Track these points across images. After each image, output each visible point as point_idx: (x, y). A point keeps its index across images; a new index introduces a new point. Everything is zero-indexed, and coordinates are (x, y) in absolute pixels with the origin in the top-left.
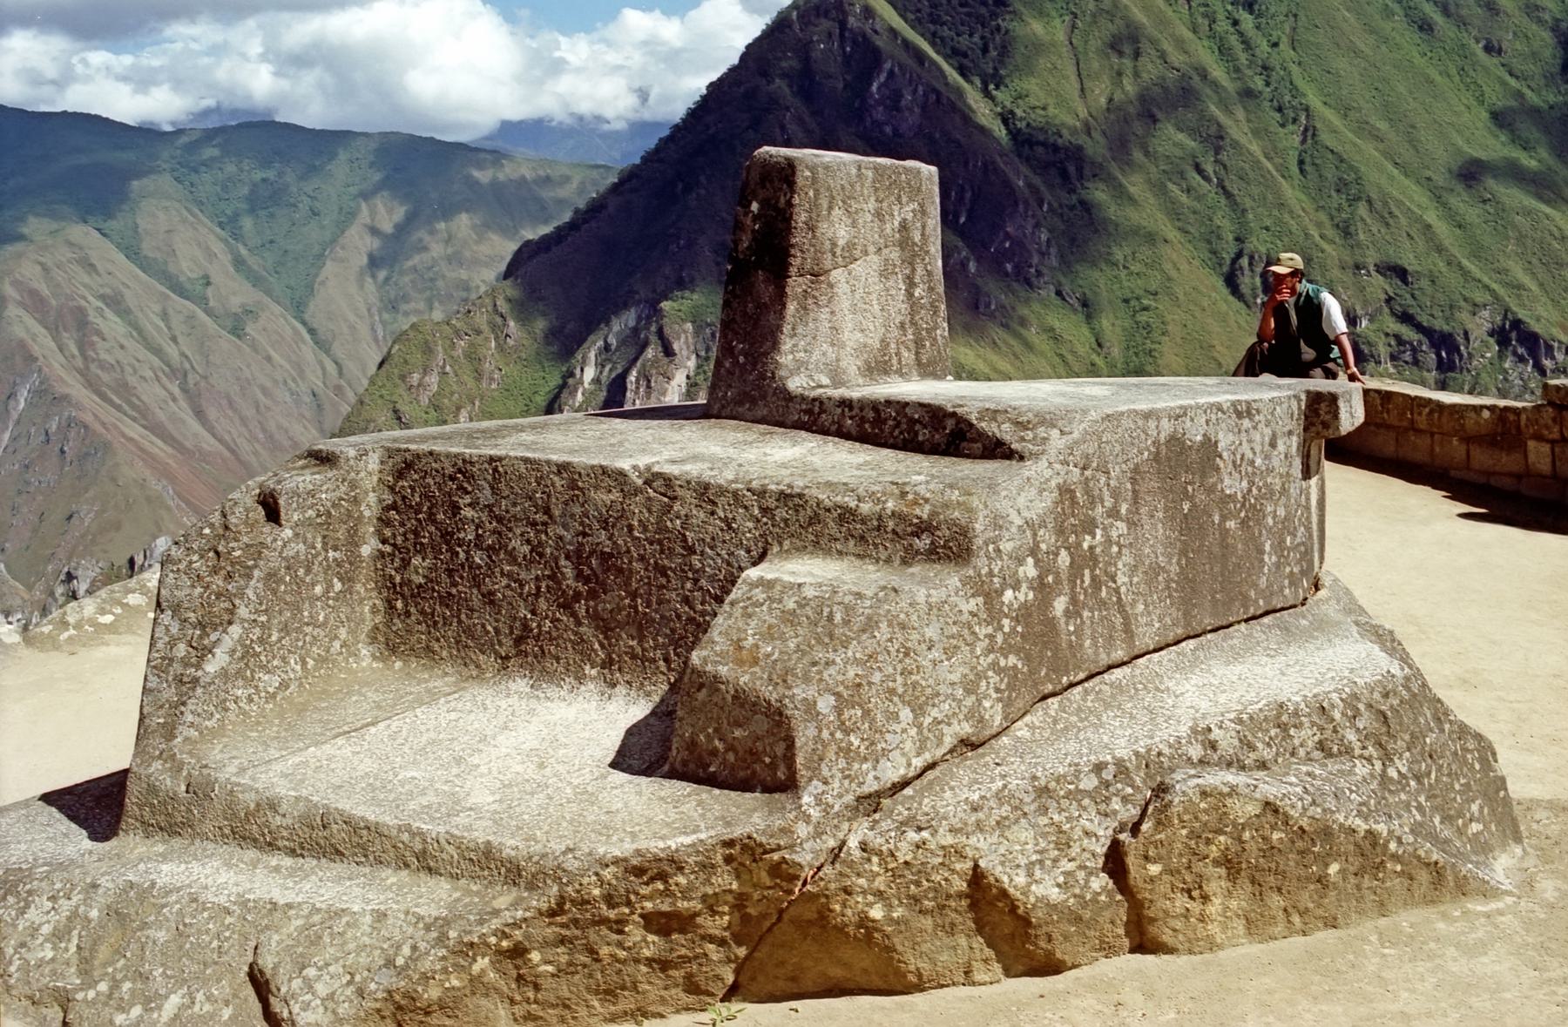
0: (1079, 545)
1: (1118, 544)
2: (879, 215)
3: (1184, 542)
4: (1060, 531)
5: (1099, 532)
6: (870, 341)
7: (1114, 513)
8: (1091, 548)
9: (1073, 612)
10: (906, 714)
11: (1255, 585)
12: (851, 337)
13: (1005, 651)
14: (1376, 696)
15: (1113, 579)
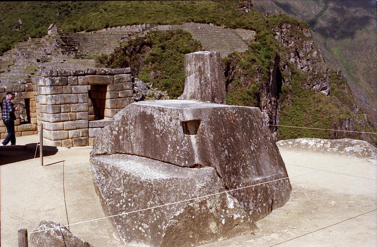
0: (125, 128)
2: (195, 65)
4: (122, 124)
5: (128, 127)
6: (192, 92)
8: (127, 129)
9: (123, 139)
10: (101, 144)
11: (165, 155)
12: (189, 90)
13: (112, 141)
14: (133, 179)
15: (130, 136)
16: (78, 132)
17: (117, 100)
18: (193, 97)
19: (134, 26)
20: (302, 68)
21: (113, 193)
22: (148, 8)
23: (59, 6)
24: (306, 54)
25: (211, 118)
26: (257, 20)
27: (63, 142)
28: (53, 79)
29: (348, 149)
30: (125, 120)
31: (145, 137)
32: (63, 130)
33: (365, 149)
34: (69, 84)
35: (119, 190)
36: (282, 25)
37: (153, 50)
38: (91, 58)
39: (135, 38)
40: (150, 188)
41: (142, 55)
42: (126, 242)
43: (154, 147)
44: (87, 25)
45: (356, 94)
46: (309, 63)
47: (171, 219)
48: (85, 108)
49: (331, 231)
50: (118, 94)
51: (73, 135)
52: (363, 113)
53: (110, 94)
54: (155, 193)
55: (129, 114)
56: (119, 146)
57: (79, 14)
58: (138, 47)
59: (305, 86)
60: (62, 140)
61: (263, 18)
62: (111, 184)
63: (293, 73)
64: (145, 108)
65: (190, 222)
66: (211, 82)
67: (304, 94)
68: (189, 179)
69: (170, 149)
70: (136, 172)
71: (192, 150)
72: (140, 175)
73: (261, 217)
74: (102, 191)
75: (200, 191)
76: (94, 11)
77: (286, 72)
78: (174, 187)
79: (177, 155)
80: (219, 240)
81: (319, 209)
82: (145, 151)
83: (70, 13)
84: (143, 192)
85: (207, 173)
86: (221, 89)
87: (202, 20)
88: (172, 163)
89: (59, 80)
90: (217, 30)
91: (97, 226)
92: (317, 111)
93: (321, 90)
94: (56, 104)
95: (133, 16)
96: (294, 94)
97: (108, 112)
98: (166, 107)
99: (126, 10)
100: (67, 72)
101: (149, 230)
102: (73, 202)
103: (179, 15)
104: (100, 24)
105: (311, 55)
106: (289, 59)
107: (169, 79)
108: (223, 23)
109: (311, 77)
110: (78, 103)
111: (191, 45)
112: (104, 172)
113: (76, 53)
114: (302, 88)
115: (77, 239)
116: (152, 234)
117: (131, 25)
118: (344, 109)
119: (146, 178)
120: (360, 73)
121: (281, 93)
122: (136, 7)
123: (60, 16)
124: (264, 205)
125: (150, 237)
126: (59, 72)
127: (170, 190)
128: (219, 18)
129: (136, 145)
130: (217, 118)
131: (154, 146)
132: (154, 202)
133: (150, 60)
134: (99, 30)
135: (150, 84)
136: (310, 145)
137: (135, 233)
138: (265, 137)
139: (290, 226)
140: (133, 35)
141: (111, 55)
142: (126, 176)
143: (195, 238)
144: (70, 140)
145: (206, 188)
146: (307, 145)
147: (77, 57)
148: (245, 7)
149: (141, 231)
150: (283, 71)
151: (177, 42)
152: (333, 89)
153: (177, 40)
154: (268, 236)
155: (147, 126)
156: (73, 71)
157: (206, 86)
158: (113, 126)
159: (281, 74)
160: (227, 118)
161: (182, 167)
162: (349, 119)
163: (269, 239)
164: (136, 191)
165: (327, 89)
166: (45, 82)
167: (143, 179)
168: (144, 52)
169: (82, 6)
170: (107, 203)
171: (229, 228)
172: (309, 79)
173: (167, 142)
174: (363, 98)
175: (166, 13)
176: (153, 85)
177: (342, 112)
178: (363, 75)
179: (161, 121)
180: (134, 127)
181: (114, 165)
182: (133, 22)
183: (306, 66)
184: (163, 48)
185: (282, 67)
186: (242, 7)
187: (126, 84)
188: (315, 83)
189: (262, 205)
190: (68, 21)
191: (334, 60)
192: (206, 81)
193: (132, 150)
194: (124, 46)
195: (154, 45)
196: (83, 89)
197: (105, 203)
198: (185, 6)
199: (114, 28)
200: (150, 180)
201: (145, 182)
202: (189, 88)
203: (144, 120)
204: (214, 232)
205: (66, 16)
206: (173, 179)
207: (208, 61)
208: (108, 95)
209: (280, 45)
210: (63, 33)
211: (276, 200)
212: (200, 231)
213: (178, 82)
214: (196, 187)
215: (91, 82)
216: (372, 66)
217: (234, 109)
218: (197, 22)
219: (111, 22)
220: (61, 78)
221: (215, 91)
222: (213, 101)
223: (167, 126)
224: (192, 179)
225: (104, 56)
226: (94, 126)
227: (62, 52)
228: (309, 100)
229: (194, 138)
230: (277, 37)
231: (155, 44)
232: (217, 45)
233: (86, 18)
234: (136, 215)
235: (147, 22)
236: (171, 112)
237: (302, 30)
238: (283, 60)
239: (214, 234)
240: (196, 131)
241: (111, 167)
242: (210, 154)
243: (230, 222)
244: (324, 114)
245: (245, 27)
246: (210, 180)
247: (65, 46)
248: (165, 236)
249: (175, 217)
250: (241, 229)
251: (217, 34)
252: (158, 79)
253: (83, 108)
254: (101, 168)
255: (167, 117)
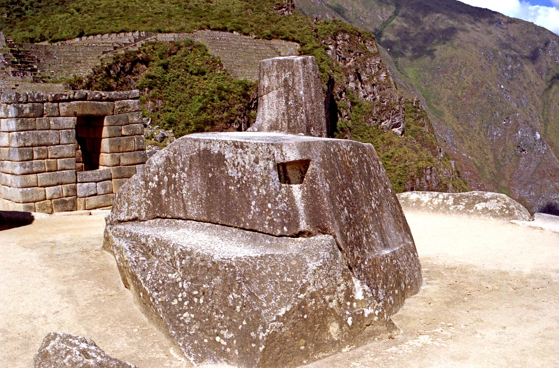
0: (171, 176)
1: (183, 180)
2: (277, 77)
3: (209, 187)
4: (166, 170)
5: (177, 174)
7: (183, 169)
8: (175, 178)
9: (168, 195)
10: (126, 204)
12: (268, 117)
13: (148, 198)
14: (198, 258)
15: (181, 190)
16: (60, 189)
17: (120, 140)
18: (274, 127)
19: (122, 34)
20: (365, 97)
21: (164, 282)
22: (142, 8)
23: (7, 3)
24: (371, 77)
25: (323, 158)
26: (302, 27)
27: (37, 206)
28: (20, 106)
29: (480, 206)
30: (170, 163)
31: (209, 191)
32: (37, 186)
33: (505, 206)
34: (45, 114)
35: (173, 277)
36: (337, 35)
37: (150, 70)
38: (57, 82)
39: (123, 52)
40: (232, 272)
41: (134, 78)
42: (196, 363)
43: (226, 206)
44: (50, 33)
45: (437, 133)
46: (375, 89)
47: (273, 321)
48: (71, 153)
49: (505, 327)
50: (121, 131)
51: (53, 194)
52: (449, 159)
53: (109, 130)
54: (240, 280)
55: (178, 154)
56: (161, 208)
57: (38, 15)
58: (128, 65)
59: (370, 122)
60: (35, 202)
61: (309, 24)
62: (157, 268)
63: (353, 104)
64: (207, 143)
65: (301, 324)
66: (305, 103)
67: (369, 133)
68: (293, 256)
69: (255, 209)
70: (201, 248)
71: (295, 210)
72: (209, 251)
73: (394, 311)
74: (144, 279)
75: (314, 274)
76: (61, 12)
77: (343, 102)
78: (270, 269)
79: (268, 218)
80: (344, 350)
81: (473, 295)
82: (208, 214)
83: (24, 14)
84: (218, 279)
85: (322, 245)
86: (319, 114)
87: (221, 26)
88: (259, 230)
89: (30, 108)
90: (244, 42)
91: (139, 338)
92: (387, 157)
93: (392, 128)
94: (25, 147)
95: (120, 19)
96: (355, 134)
97: (105, 158)
98: (247, 141)
99: (109, 11)
100: (43, 96)
101: (235, 342)
102: (86, 300)
103: (188, 19)
104: (70, 31)
105: (377, 78)
106: (348, 83)
107: (174, 112)
108: (252, 31)
109: (378, 109)
110: (59, 144)
111: (207, 63)
112: (141, 248)
113: (35, 74)
114: (365, 125)
115: (120, 362)
116: (241, 347)
117: (118, 33)
118: (424, 154)
119: (222, 257)
120: (444, 104)
121: (337, 131)
122: (125, 7)
123: (9, 18)
124: (396, 291)
125: (237, 353)
126: (29, 96)
127: (264, 274)
128: (247, 24)
129: (192, 204)
130: (331, 158)
131: (226, 204)
132: (239, 294)
133: (146, 84)
134: (68, 39)
135: (148, 120)
136: (422, 202)
137: (209, 347)
138: (385, 188)
139: (442, 323)
140: (121, 47)
141: (88, 77)
142: (184, 254)
143: (308, 349)
144: (48, 202)
145: (323, 269)
146: (418, 201)
147: (35, 81)
148: (284, 9)
149: (220, 343)
150: (338, 100)
151: (185, 58)
152: (408, 126)
153: (186, 56)
154: (415, 340)
155: (213, 173)
156: (51, 95)
157: (297, 109)
158: (149, 175)
159: (336, 104)
160: (342, 158)
161: (276, 236)
162: (431, 169)
163: (420, 345)
164: (207, 278)
165: (400, 126)
166: (6, 111)
167: (216, 258)
168: (137, 72)
169: (42, 4)
170: (154, 300)
171: (358, 332)
172: (375, 112)
173: (249, 197)
174: (448, 138)
175: (169, 15)
176: (151, 121)
177: (421, 159)
178: (448, 106)
179: (238, 163)
180: (188, 175)
181: (159, 237)
182: (120, 28)
183: (370, 93)
184: (165, 67)
185: (338, 95)
186: (279, 9)
187: (132, 115)
188: (384, 118)
189: (394, 292)
190: (22, 26)
191: (409, 86)
192: (297, 102)
193: (186, 212)
194: (108, 64)
195: (151, 63)
196: (67, 122)
197: (151, 300)
198: (196, 5)
199: (91, 37)
200: (228, 259)
201: (221, 262)
202: (266, 113)
203: (206, 164)
204: (336, 339)
205: (18, 19)
206: (267, 256)
207: (301, 70)
208: (105, 132)
209: (334, 64)
210: (14, 45)
211: (409, 284)
212: (315, 338)
213: (188, 117)
214: (308, 267)
215: (79, 112)
216: (459, 94)
217: (348, 144)
218: (215, 29)
219: (88, 27)
220: (33, 105)
221: (310, 118)
222: (308, 133)
223: (250, 172)
224: (298, 256)
225: (78, 78)
226: (85, 180)
227: (12, 72)
228: (377, 142)
229: (297, 189)
230: (329, 53)
231: (153, 61)
232: (245, 63)
233: (50, 22)
234: (209, 318)
235: (140, 29)
236: (256, 149)
237: (364, 42)
238: (338, 85)
239: (336, 342)
240: (303, 178)
241: (153, 240)
242: (325, 215)
243: (360, 321)
244: (397, 161)
245: (284, 37)
246: (328, 256)
247: (17, 63)
248: (264, 350)
249: (278, 317)
250: (373, 331)
251: (244, 47)
252: (158, 113)
253: (67, 152)
254: (134, 242)
255: (249, 157)
